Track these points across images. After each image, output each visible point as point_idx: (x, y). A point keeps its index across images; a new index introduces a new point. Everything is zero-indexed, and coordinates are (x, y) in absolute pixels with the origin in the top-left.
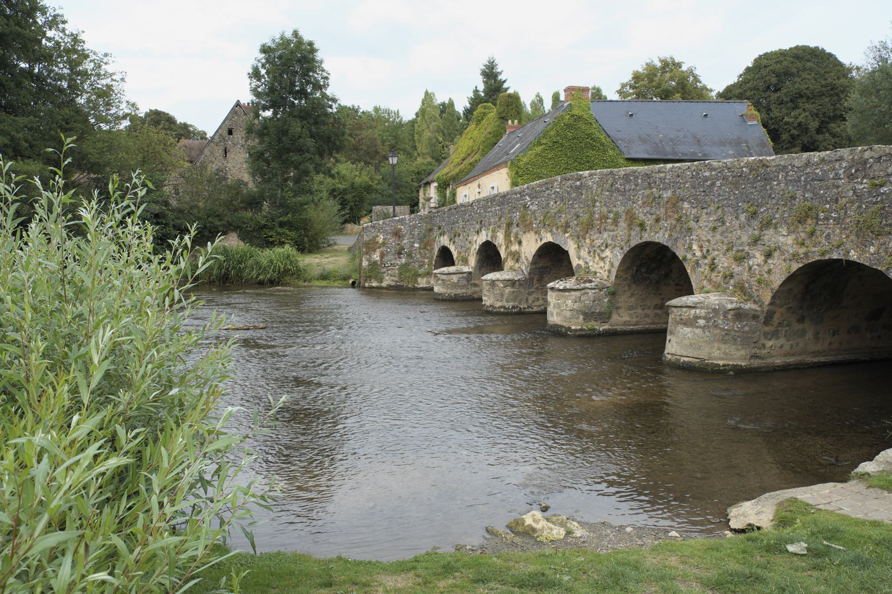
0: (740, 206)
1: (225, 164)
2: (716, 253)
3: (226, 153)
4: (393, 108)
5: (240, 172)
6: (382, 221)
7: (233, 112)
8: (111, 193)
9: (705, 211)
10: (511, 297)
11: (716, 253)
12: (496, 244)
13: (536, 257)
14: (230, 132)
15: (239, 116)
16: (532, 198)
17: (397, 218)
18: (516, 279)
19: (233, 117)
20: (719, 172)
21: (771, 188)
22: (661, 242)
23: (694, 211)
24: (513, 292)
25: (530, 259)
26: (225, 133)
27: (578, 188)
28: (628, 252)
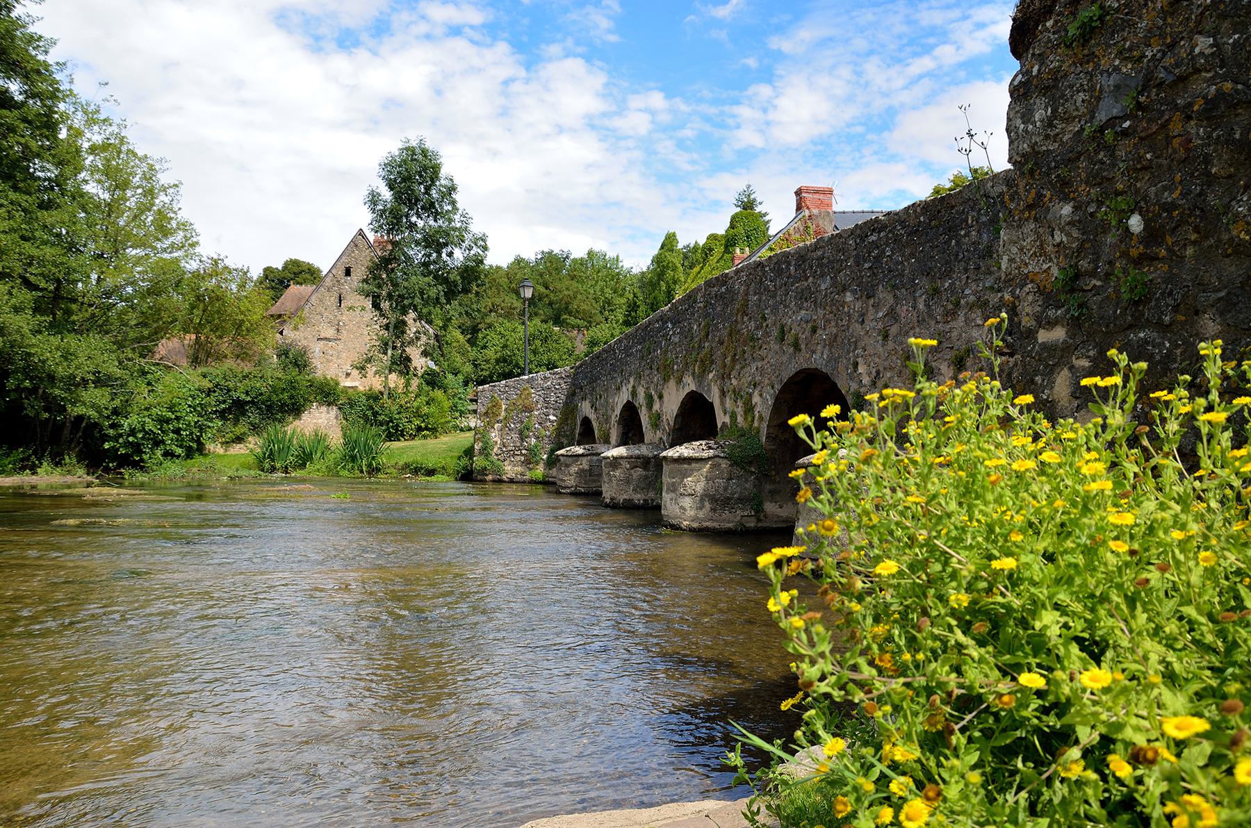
0: (917, 284)
1: (339, 317)
2: (889, 375)
3: (340, 301)
4: (611, 254)
5: (359, 327)
6: (504, 382)
7: (354, 244)
8: (1204, 685)
9: (872, 301)
10: (642, 485)
11: (889, 375)
12: (637, 405)
13: (680, 419)
14: (348, 272)
15: (361, 251)
16: (674, 324)
17: (526, 377)
18: (651, 455)
19: (353, 252)
20: (890, 231)
21: (958, 243)
22: (819, 367)
23: (858, 305)
24: (646, 477)
25: (672, 423)
26: (341, 272)
27: (722, 296)
28: (780, 392)
